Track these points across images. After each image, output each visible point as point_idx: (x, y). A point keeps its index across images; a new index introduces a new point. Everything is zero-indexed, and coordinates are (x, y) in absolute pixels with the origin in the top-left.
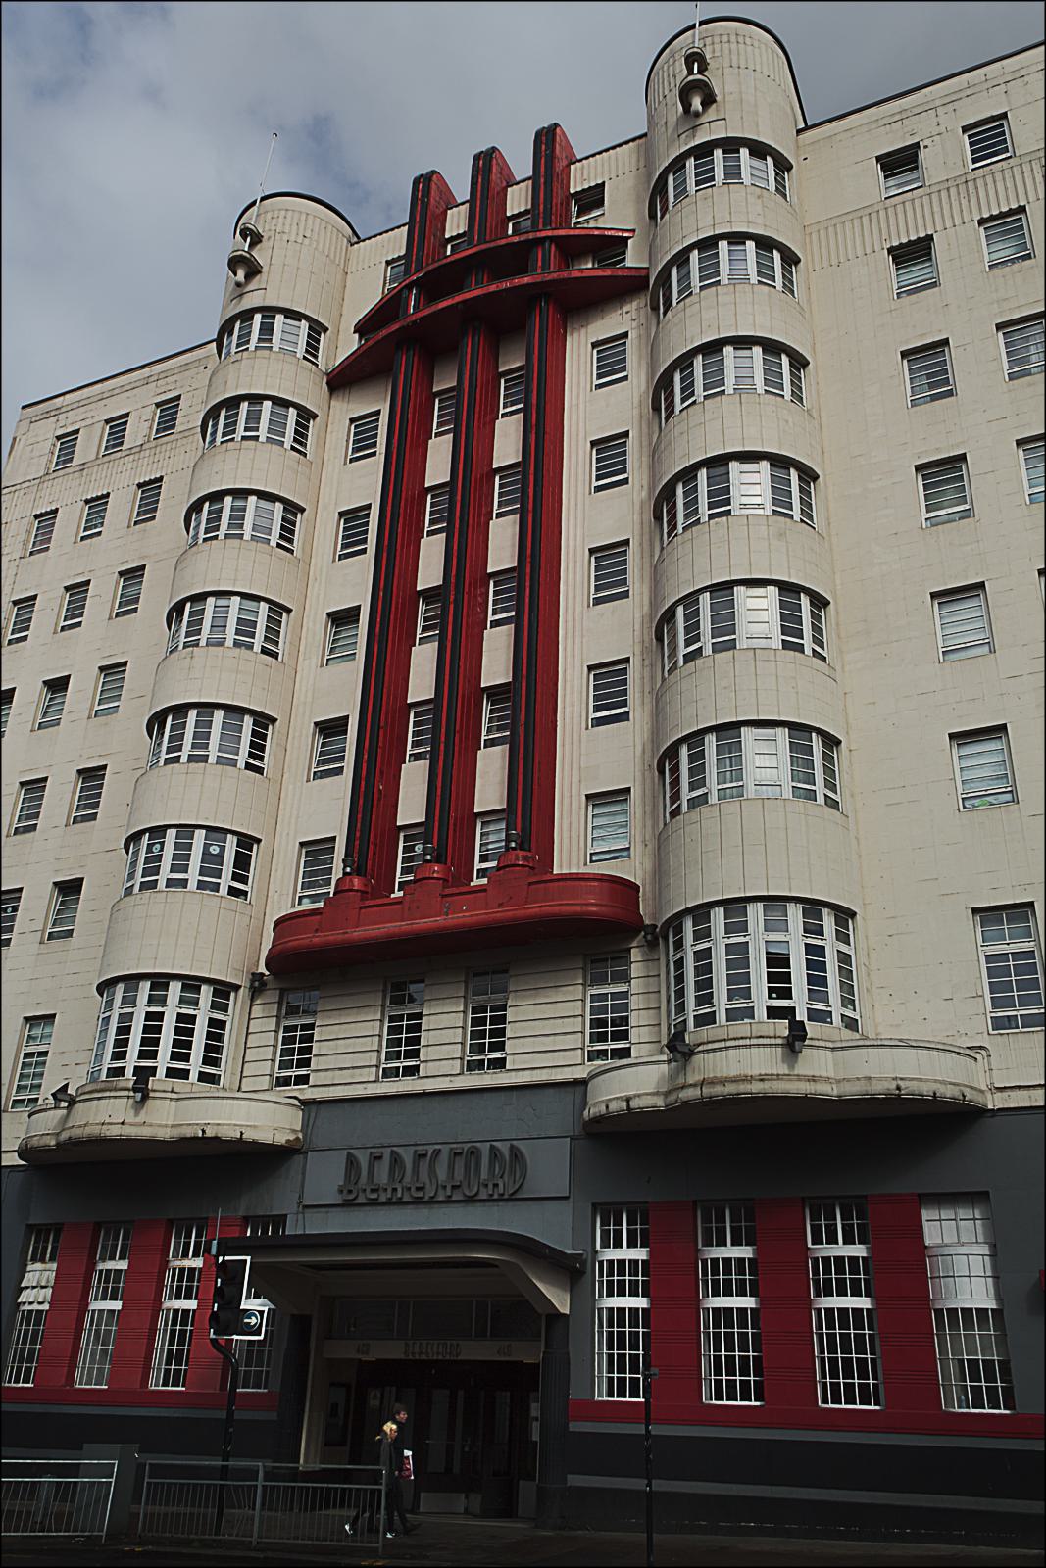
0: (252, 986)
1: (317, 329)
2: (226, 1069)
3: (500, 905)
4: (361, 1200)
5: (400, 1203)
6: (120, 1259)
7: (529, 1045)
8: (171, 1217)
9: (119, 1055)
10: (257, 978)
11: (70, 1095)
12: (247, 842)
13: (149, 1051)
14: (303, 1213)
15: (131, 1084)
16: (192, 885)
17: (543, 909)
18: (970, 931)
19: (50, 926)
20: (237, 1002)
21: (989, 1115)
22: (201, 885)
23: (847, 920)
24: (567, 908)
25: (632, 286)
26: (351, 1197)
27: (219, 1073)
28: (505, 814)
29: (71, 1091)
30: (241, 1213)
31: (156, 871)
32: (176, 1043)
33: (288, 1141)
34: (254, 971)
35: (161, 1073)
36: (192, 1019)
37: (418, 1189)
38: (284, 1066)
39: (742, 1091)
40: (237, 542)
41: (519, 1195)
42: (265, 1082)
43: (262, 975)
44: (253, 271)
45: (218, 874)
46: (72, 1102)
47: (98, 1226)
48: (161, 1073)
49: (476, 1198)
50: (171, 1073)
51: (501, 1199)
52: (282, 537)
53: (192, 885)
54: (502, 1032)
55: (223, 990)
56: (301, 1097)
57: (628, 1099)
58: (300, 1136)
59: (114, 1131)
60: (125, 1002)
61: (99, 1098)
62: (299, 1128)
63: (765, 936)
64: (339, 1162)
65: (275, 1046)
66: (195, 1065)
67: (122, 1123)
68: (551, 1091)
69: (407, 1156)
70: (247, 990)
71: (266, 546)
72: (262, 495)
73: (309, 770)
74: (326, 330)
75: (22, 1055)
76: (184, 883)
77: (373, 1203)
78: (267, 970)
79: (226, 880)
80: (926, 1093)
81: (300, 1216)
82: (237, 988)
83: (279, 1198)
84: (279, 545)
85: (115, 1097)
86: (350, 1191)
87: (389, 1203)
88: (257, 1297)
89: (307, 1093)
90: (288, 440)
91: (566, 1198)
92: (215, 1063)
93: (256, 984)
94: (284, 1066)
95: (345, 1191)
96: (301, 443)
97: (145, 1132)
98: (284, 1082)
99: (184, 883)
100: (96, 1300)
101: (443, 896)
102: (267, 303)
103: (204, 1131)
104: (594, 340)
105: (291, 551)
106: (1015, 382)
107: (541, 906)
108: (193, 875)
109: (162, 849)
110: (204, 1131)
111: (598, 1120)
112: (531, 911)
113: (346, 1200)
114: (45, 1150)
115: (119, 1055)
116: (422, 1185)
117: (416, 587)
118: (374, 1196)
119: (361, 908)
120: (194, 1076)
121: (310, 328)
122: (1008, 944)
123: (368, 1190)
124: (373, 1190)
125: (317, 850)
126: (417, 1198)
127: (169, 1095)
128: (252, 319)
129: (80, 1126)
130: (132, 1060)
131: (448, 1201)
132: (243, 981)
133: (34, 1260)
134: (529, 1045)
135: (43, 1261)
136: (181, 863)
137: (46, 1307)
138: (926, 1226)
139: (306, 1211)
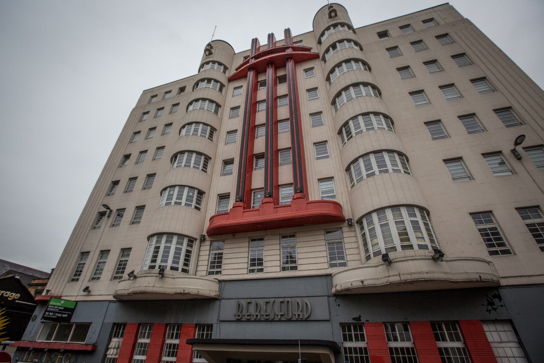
0: (201, 239)
1: (226, 68)
2: (191, 268)
3: (297, 211)
4: (244, 319)
5: (260, 321)
6: (147, 338)
7: (306, 261)
8: (168, 322)
9: (154, 261)
10: (203, 237)
11: (134, 275)
12: (201, 193)
13: (165, 260)
14: (220, 324)
15: (157, 272)
16: (183, 204)
17: (293, 214)
18: (470, 221)
19: (133, 220)
20: (196, 245)
21: (501, 288)
22: (186, 204)
23: (423, 211)
24: (223, 223)
25: (316, 57)
26: (239, 318)
27: (189, 269)
28: (265, 189)
29: (135, 273)
30: (195, 322)
31: (171, 199)
32: (174, 257)
33: (215, 295)
34: (201, 234)
35: (168, 268)
36: (181, 249)
37: (267, 315)
38: (211, 267)
39: (420, 278)
40: (203, 110)
41: (309, 319)
42: (204, 273)
43: (205, 236)
44: (210, 53)
45: (192, 201)
46: (135, 277)
47: (139, 325)
48: (168, 268)
49: (291, 320)
50: (172, 268)
51: (302, 320)
52: (203, 167)
53: (183, 204)
54: (221, 262)
55: (191, 240)
56: (218, 279)
57: (362, 282)
58: (218, 293)
59: (150, 289)
60: (157, 242)
61: (145, 276)
62: (218, 291)
63: (409, 219)
64: (234, 303)
65: (208, 260)
66: (181, 266)
67: (153, 286)
68: (317, 278)
69: (262, 302)
70: (199, 241)
71: (198, 170)
72: (205, 124)
73: (221, 173)
74: (228, 69)
75: (119, 261)
76: (180, 203)
77: (248, 321)
78: (207, 234)
79: (194, 204)
80: (490, 279)
81: (218, 325)
82: (196, 239)
83: (211, 317)
84: (202, 170)
85: (151, 276)
86: (239, 316)
87: (255, 321)
88: (200, 357)
89: (220, 277)
90: (201, 167)
91: (328, 320)
92: (199, 204)
93: (202, 239)
94: (211, 267)
95: (237, 316)
96: (211, 137)
97: (162, 290)
98: (210, 273)
99: (180, 203)
100: (136, 355)
101: (274, 208)
102: (214, 60)
103: (184, 290)
104: (304, 69)
105: (206, 172)
106: (415, 73)
107: (299, 212)
108: (184, 201)
109: (174, 192)
110: (184, 290)
111: (337, 291)
112: (309, 212)
113: (237, 319)
114: (122, 295)
115: (154, 261)
116: (268, 314)
117: (255, 124)
118: (249, 318)
119: (243, 212)
120: (180, 270)
121: (205, 158)
122: (485, 225)
123: (246, 316)
124: (248, 316)
125: (223, 197)
126: (266, 319)
127: (171, 276)
128: (211, 81)
129: (137, 287)
130: (158, 263)
131: (280, 321)
132: (198, 237)
133: (115, 336)
134: (306, 261)
135: (118, 337)
136: (180, 197)
137: (117, 356)
138: (488, 334)
139: (221, 323)
